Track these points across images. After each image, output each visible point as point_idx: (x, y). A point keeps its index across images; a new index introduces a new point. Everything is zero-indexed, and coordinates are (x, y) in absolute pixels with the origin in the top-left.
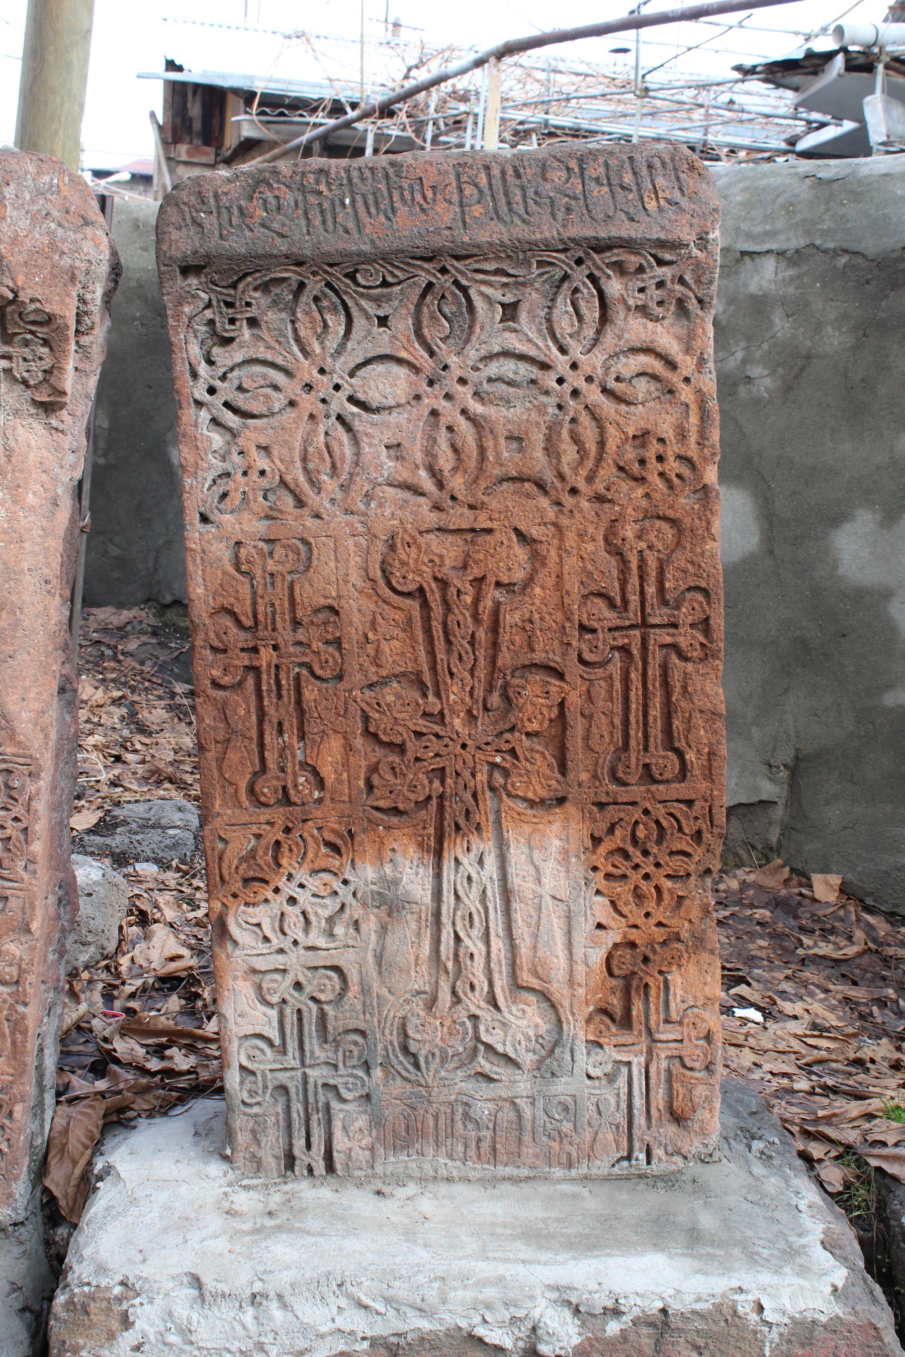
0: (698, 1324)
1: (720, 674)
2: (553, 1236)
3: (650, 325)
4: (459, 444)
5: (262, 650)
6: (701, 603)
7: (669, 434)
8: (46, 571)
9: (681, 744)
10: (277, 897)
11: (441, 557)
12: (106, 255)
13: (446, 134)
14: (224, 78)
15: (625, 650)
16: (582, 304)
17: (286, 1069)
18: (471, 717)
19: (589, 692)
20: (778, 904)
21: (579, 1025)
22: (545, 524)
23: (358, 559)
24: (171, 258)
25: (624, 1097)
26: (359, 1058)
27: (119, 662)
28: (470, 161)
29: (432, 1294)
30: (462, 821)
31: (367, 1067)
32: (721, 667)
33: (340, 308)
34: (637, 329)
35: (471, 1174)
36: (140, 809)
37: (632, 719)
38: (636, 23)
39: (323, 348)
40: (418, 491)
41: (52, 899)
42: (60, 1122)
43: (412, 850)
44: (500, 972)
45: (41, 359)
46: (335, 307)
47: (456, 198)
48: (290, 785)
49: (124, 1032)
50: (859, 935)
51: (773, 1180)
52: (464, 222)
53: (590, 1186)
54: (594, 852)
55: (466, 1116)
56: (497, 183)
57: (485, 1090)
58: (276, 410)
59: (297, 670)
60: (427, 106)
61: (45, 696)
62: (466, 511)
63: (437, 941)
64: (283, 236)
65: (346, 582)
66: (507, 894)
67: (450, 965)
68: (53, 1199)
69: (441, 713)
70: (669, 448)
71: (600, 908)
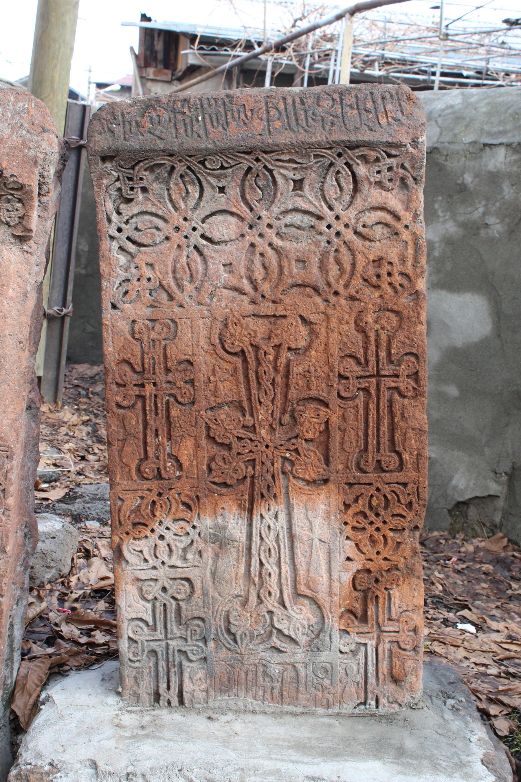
1: (425, 406)
2: (313, 748)
3: (384, 193)
4: (267, 264)
5: (147, 386)
6: (413, 363)
7: (395, 260)
8: (20, 336)
9: (400, 448)
10: (153, 535)
11: (255, 332)
13: (319, 62)
14: (177, 25)
16: (342, 180)
17: (156, 640)
18: (272, 429)
19: (343, 415)
20: (498, 561)
21: (335, 619)
22: (318, 313)
23: (205, 332)
24: (95, 151)
25: (362, 665)
26: (200, 635)
27: (90, 398)
28: (274, 94)
30: (265, 492)
31: (205, 640)
32: (426, 402)
33: (196, 181)
34: (376, 196)
35: (267, 709)
36: (92, 488)
37: (370, 432)
39: (186, 206)
41: (20, 533)
42: (23, 671)
43: (234, 508)
44: (287, 585)
45: (17, 210)
46: (193, 182)
47: (265, 117)
48: (162, 468)
49: (69, 620)
51: (457, 723)
52: (270, 131)
53: (340, 720)
54: (345, 513)
55: (265, 673)
56: (290, 108)
57: (276, 657)
58: (158, 242)
59: (167, 398)
60: (307, 44)
61: (18, 411)
62: (271, 304)
64: (161, 139)
65: (198, 346)
66: (292, 537)
67: (257, 580)
68: (16, 717)
69: (254, 426)
70: (395, 268)
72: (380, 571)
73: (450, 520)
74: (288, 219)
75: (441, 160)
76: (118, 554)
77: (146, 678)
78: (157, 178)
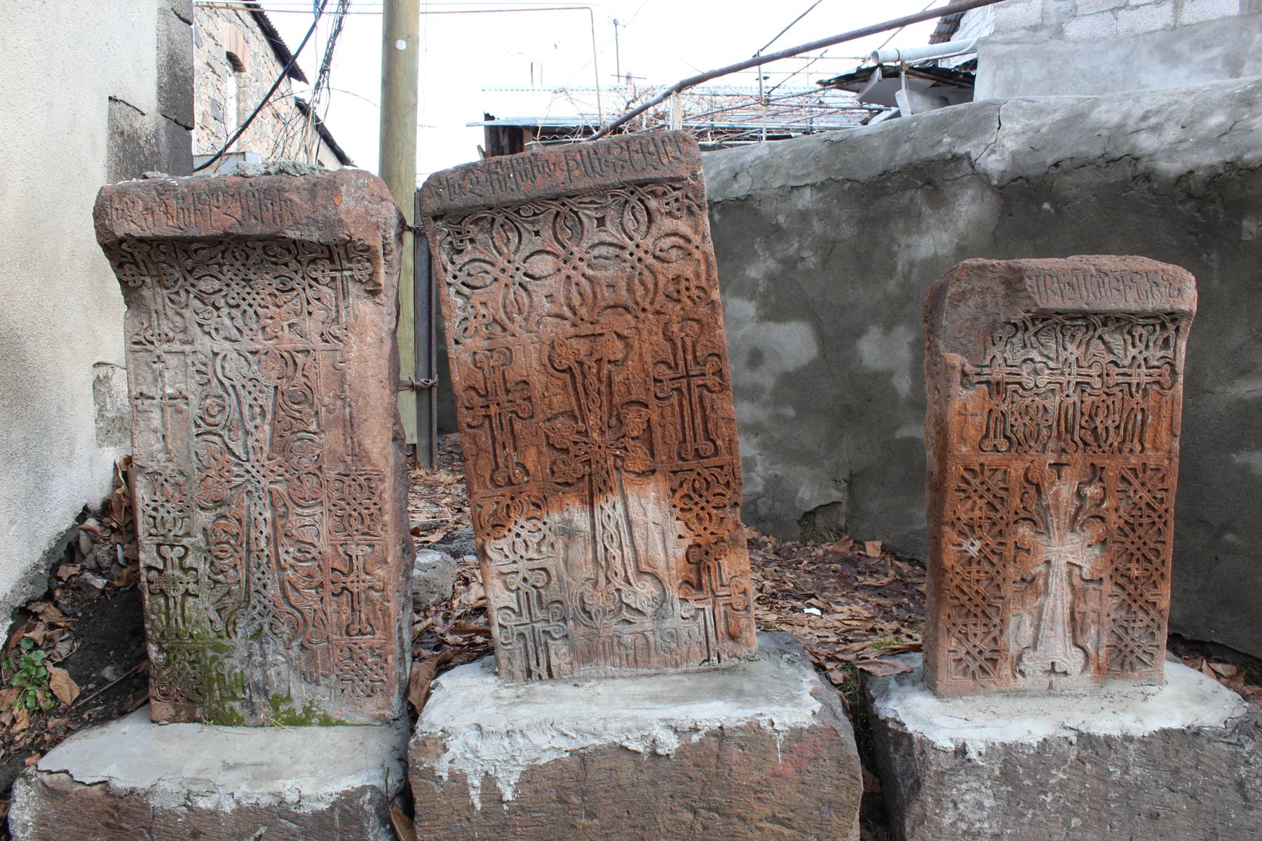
0: (740, 734)
7: (691, 276)
9: (713, 437)
12: (394, 214)
15: (679, 390)
18: (602, 432)
20: (846, 560)
29: (599, 726)
31: (565, 620)
34: (668, 224)
38: (758, 61)
40: (563, 318)
41: (398, 547)
49: (452, 632)
50: (892, 572)
57: (627, 629)
63: (595, 551)
66: (629, 523)
68: (413, 707)
71: (680, 527)
72: (709, 544)
73: (800, 530)
74: (596, 252)
75: (756, 205)
76: (482, 554)
77: (518, 657)
78: (481, 230)
